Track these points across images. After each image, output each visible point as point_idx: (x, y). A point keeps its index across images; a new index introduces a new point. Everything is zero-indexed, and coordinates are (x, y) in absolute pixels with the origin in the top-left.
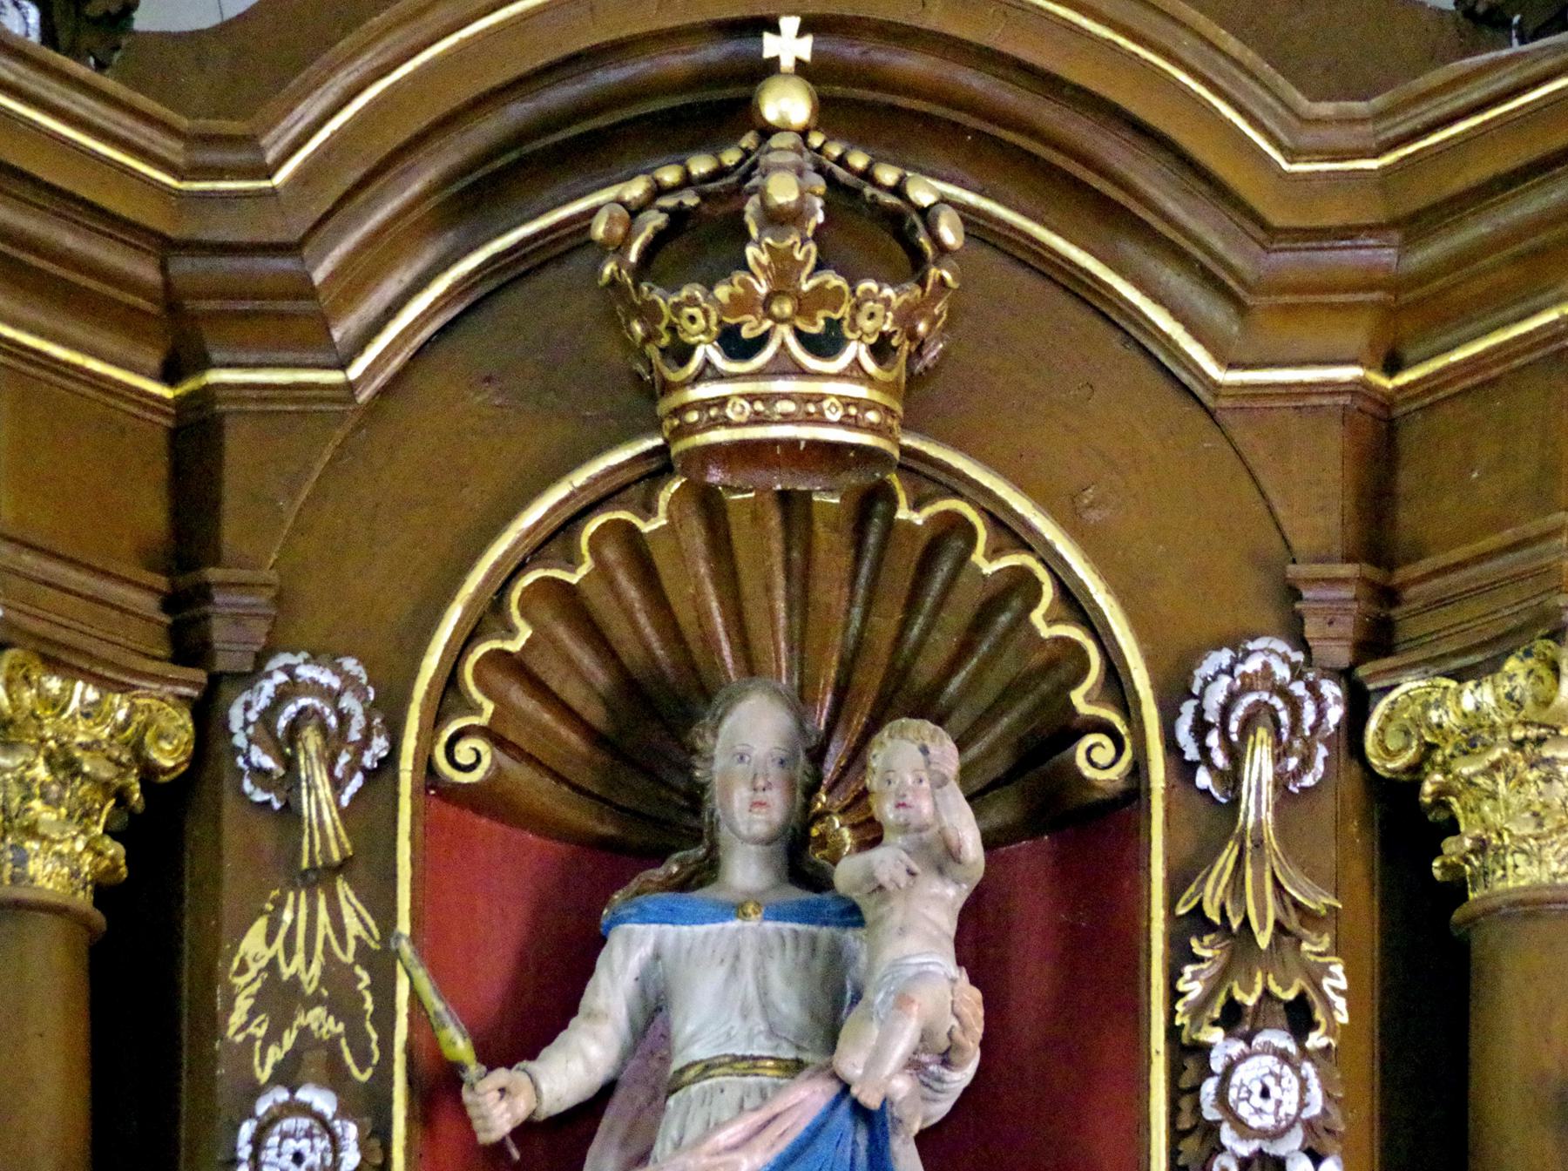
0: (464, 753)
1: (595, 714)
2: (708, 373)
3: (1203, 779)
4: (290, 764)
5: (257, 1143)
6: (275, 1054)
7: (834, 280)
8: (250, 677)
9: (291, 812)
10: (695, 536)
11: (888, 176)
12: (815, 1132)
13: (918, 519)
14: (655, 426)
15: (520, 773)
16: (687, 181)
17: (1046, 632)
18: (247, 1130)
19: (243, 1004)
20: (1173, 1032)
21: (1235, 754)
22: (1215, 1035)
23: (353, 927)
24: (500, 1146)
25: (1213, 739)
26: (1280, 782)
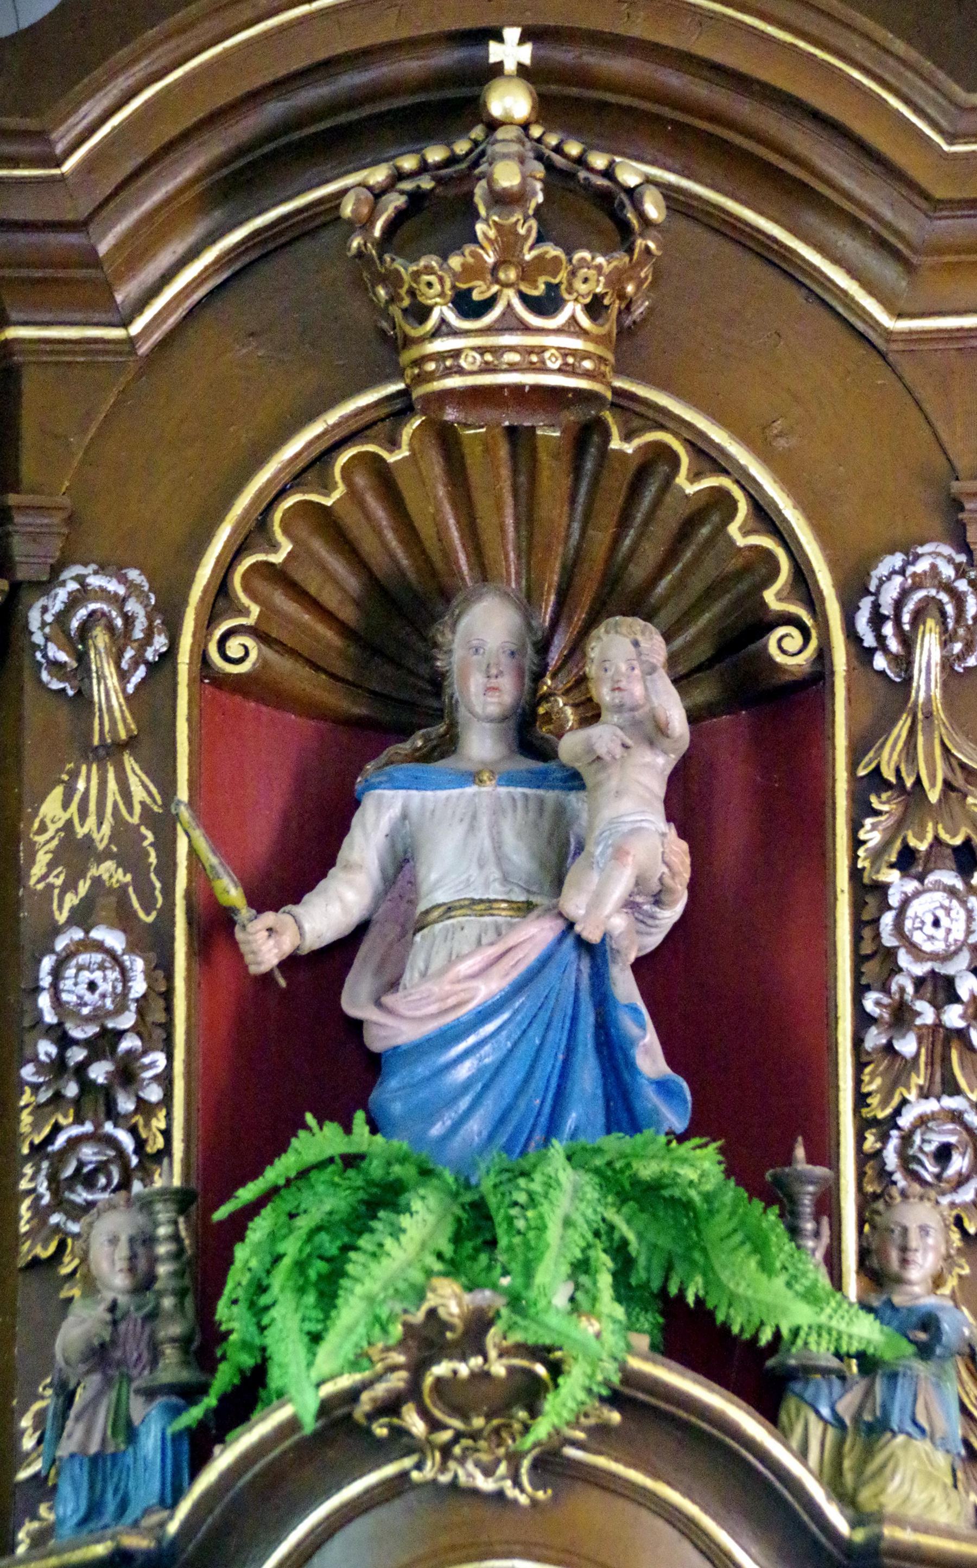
0: (234, 647)
1: (348, 614)
2: (443, 330)
3: (880, 662)
4: (82, 658)
5: (57, 973)
6: (71, 900)
7: (552, 251)
8: (46, 586)
9: (83, 699)
10: (435, 466)
11: (599, 161)
12: (545, 961)
13: (629, 448)
14: (399, 374)
15: (283, 664)
16: (424, 168)
17: (741, 542)
18: (47, 963)
19: (43, 858)
20: (855, 874)
21: (907, 642)
22: (892, 876)
23: (138, 794)
24: (267, 978)
25: (888, 629)
26: (947, 664)
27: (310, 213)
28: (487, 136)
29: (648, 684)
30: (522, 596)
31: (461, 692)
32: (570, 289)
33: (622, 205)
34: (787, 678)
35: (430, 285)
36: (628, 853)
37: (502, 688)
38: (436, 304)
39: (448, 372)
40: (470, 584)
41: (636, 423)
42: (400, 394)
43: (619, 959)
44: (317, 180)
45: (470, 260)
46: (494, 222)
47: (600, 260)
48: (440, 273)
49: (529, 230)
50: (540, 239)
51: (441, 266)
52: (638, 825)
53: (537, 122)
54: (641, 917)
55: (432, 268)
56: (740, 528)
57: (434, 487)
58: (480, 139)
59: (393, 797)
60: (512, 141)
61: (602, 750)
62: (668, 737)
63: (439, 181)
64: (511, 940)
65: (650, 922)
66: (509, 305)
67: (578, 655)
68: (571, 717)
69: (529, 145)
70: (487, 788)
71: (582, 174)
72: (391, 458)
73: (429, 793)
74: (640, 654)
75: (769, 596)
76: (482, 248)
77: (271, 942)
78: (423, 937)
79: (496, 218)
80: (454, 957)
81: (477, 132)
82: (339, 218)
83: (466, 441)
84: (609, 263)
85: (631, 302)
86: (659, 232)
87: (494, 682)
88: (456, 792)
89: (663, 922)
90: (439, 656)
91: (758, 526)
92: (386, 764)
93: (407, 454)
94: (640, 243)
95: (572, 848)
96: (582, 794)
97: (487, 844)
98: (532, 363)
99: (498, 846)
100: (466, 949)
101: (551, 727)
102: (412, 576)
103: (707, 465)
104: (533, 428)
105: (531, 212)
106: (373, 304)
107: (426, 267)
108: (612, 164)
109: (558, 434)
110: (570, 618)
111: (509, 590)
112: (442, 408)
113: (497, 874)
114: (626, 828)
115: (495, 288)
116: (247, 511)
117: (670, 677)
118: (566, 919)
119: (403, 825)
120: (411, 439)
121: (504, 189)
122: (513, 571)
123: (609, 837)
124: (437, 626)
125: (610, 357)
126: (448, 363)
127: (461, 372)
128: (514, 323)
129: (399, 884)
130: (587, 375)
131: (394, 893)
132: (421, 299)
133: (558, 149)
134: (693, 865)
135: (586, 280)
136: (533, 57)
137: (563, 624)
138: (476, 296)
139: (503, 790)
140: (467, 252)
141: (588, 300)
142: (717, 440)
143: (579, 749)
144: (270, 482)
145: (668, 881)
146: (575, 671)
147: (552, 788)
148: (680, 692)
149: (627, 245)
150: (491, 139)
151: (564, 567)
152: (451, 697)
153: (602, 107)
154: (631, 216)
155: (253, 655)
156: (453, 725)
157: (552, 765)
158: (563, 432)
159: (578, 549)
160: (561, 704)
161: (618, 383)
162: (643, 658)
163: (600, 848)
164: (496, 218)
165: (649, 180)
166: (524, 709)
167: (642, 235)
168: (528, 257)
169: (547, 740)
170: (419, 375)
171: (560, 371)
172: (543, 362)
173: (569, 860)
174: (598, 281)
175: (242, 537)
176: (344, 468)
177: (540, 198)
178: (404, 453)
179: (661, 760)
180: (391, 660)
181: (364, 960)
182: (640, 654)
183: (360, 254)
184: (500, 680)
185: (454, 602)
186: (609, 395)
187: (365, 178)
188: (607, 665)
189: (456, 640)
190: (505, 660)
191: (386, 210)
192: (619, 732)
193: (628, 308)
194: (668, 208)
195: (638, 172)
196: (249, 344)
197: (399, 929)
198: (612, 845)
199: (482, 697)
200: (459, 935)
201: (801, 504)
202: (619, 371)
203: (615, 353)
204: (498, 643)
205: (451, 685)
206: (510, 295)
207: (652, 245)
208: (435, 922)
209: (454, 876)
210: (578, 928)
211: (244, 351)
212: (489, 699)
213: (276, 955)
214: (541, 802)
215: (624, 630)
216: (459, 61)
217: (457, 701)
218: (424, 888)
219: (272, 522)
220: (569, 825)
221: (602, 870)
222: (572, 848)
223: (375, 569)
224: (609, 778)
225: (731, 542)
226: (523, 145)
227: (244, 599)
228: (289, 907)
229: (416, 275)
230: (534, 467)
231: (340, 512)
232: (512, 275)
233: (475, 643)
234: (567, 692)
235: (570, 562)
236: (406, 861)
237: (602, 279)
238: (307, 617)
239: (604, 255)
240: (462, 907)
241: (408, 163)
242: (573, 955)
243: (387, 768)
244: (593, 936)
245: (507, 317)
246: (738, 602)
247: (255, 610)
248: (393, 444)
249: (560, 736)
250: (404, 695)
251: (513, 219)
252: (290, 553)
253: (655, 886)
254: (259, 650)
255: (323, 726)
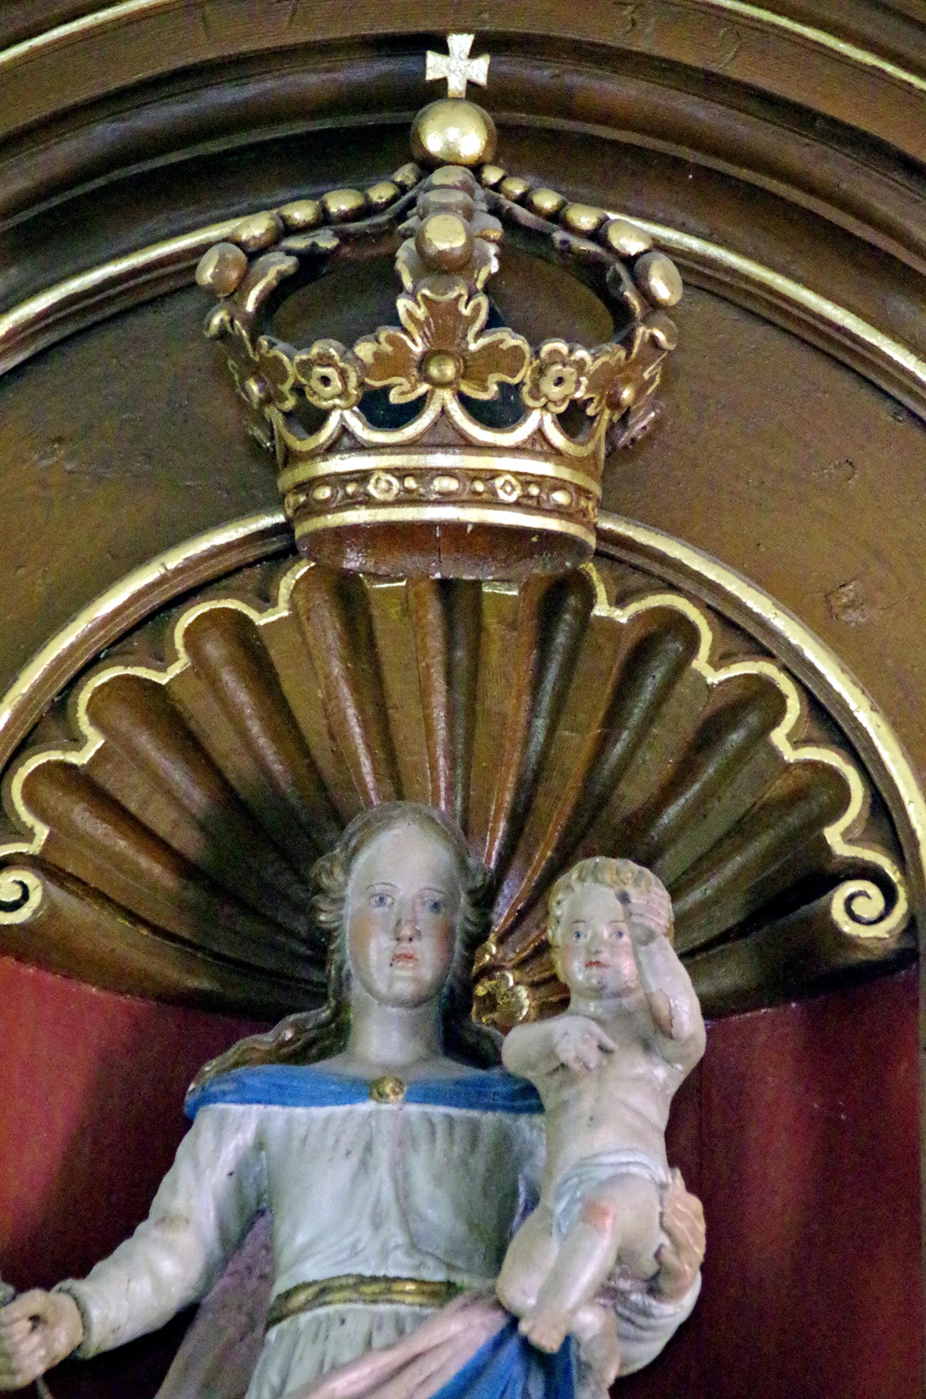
7: (510, 339)
11: (585, 218)
13: (622, 616)
14: (278, 502)
16: (324, 219)
17: (790, 755)
27: (154, 274)
28: (419, 178)
29: (643, 959)
30: (457, 823)
31: (355, 961)
32: (536, 393)
33: (618, 280)
34: (861, 956)
35: (325, 380)
36: (604, 1213)
37: (419, 956)
38: (334, 407)
39: (352, 502)
40: (376, 802)
41: (635, 580)
42: (276, 530)
43: (591, 1379)
44: (165, 231)
45: (388, 348)
46: (424, 297)
47: (582, 353)
48: (341, 365)
49: (477, 309)
50: (493, 321)
51: (343, 356)
52: (624, 1169)
53: (495, 163)
54: (627, 1313)
55: (331, 357)
56: (789, 737)
57: (329, 663)
58: (409, 182)
59: (243, 1115)
60: (455, 187)
61: (567, 1054)
62: (671, 1037)
63: (345, 238)
64: (419, 1343)
65: (641, 1320)
66: (444, 412)
67: (538, 913)
68: (527, 1003)
69: (480, 193)
70: (391, 1106)
71: (559, 236)
72: (261, 620)
73: (300, 1111)
74: (629, 914)
75: (833, 835)
76: (405, 331)
77: (36, 1339)
78: (280, 1336)
79: (427, 292)
80: (326, 1368)
81: (406, 174)
82: (194, 284)
83: (373, 597)
84: (595, 358)
85: (628, 413)
86: (671, 317)
87: (405, 947)
88: (341, 1110)
89: (662, 1321)
90: (322, 906)
91: (816, 734)
92: (236, 1065)
93: (286, 613)
94: (642, 332)
95: (521, 1200)
96: (538, 1119)
97: (387, 1192)
98: (476, 493)
99: (403, 1195)
100: (347, 1356)
101: (495, 1016)
102: (285, 784)
103: (736, 644)
104: (477, 584)
105: (479, 285)
106: (243, 405)
107: (321, 356)
108: (603, 223)
109: (515, 593)
110: (529, 859)
111: (435, 814)
112: (339, 553)
113: (400, 1238)
114: (603, 1174)
115: (424, 388)
116: (38, 688)
117: (676, 949)
118: (507, 1312)
119: (258, 1159)
120: (293, 592)
121: (441, 253)
122: (443, 785)
123: (576, 1187)
124: (321, 862)
125: (596, 488)
126: (350, 489)
127: (369, 502)
128: (451, 436)
129: (248, 1249)
130: (558, 511)
131: (235, 1265)
132: (313, 400)
133: (524, 200)
134: (709, 1235)
135: (560, 381)
136: (491, 72)
137: (517, 863)
138: (394, 398)
139: (414, 1109)
140: (382, 338)
141: (562, 409)
142: (756, 609)
143: (533, 1053)
144: (73, 648)
145: (669, 1256)
146: (535, 933)
147: (492, 1108)
148: (690, 974)
149: (624, 333)
150: (425, 183)
151: (520, 783)
152: (340, 969)
153: (594, 144)
154: (630, 294)
155: (36, 898)
156: (341, 1009)
157: (495, 1072)
158: (523, 589)
159: (544, 754)
160: (511, 983)
161: (606, 525)
162: (635, 919)
163: (563, 1204)
164: (427, 292)
165: (658, 246)
166: (452, 990)
167: (645, 321)
168: (473, 347)
169: (488, 1036)
170: (304, 505)
171: (517, 505)
172: (494, 493)
173: (517, 1219)
174: (578, 383)
175: (27, 727)
176: (188, 632)
177: (494, 266)
178: (282, 611)
179: (661, 1073)
180: (251, 911)
181: (187, 1368)
182: (629, 914)
183: (223, 334)
184: (416, 944)
185: (350, 828)
186: (592, 541)
187: (236, 230)
188: (581, 927)
189: (351, 884)
190: (425, 916)
191: (265, 275)
192: (596, 1029)
193: (624, 419)
194: (686, 284)
195: (641, 233)
196: (53, 453)
197: (243, 1319)
198: (581, 1199)
199: (387, 970)
200: (336, 1331)
201: (880, 704)
202: (604, 507)
203: (603, 480)
204: (414, 891)
205: (339, 950)
206: (446, 396)
207: (661, 336)
208: (302, 1309)
209: (333, 1238)
210: (524, 1327)
211: (45, 463)
212: (397, 972)
213: (42, 1360)
214: (474, 1129)
215: (607, 877)
216: (380, 77)
217: (349, 975)
218: (285, 1257)
219: (76, 704)
220: (517, 1165)
221: (565, 1238)
222: (521, 1200)
223: (231, 777)
224: (579, 1096)
225: (774, 754)
226: (470, 191)
227: (27, 817)
228: (69, 1283)
229: (306, 367)
230: (478, 639)
231: (179, 692)
232: (450, 370)
233: (378, 889)
234: (522, 964)
235: (530, 775)
236: (261, 1213)
237: (584, 380)
238: (122, 843)
239: (588, 347)
240: (342, 1288)
241: (301, 213)
242: (517, 1369)
243: (239, 1071)
244: (550, 1342)
245: (442, 428)
246: (792, 837)
247: (42, 832)
248: (266, 599)
249: (506, 1031)
250: (269, 962)
251: (453, 295)
252: (99, 752)
253: (649, 1266)
254: (46, 895)
255: (138, 1004)
